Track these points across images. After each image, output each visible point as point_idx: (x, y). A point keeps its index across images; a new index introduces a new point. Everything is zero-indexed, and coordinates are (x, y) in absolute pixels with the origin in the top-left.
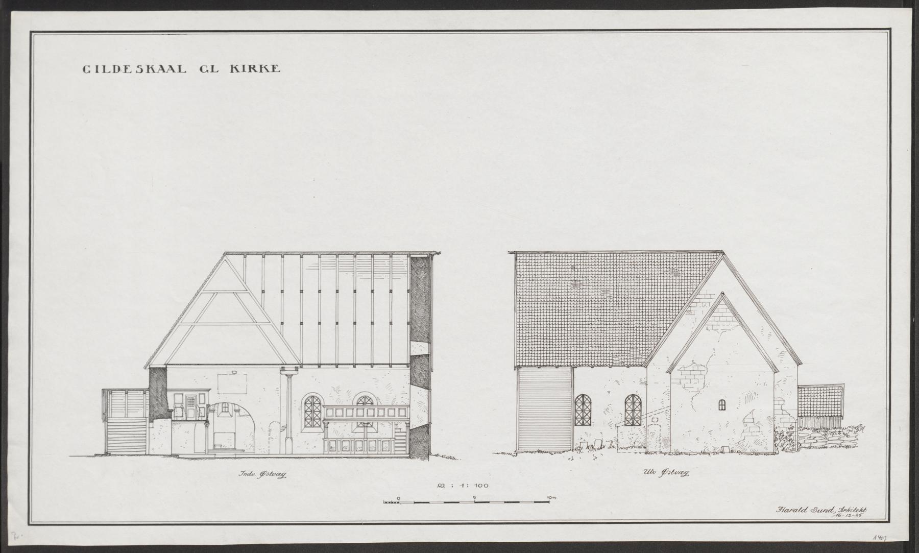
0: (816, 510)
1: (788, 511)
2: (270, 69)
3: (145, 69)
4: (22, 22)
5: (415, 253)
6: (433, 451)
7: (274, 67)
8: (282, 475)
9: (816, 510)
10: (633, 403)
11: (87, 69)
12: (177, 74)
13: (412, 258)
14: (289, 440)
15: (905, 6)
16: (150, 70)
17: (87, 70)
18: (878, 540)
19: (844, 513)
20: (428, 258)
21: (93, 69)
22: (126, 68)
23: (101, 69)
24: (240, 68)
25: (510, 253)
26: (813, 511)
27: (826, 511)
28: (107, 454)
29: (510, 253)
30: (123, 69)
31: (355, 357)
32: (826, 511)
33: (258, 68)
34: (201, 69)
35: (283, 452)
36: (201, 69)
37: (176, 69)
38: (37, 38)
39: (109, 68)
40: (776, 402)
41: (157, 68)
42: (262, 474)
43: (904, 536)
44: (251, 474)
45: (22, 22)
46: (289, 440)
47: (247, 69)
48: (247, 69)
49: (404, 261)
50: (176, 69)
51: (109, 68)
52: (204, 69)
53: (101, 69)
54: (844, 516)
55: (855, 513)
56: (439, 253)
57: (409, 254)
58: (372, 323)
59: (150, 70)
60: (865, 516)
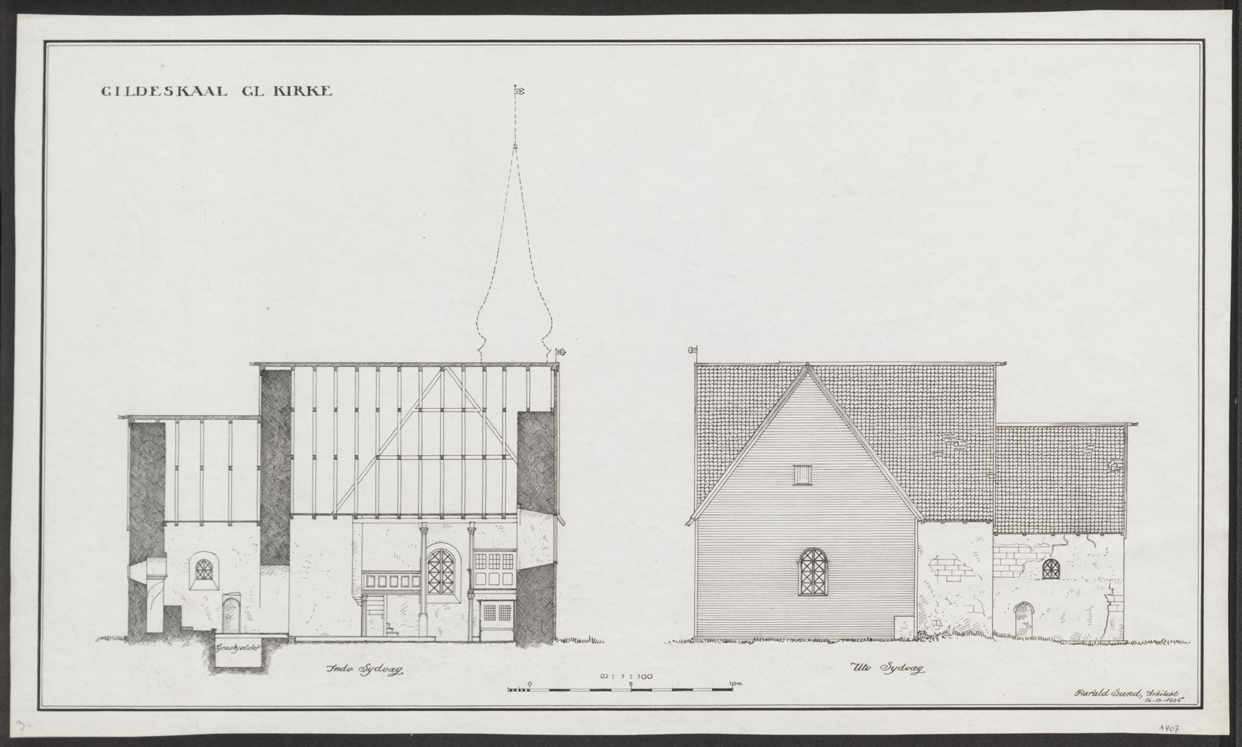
1: (1086, 694)
2: (320, 91)
3: (176, 92)
4: (32, 29)
5: (268, 364)
6: (560, 634)
7: (324, 89)
11: (107, 91)
12: (216, 97)
14: (423, 617)
19: (1154, 698)
21: (114, 91)
22: (153, 90)
24: (285, 91)
25: (251, 364)
26: (1113, 695)
27: (1095, 694)
29: (251, 364)
30: (149, 92)
31: (314, 504)
32: (1130, 694)
33: (305, 91)
34: (103, 92)
35: (423, 633)
36: (103, 92)
37: (215, 91)
38: (50, 47)
39: (133, 91)
40: (996, 550)
41: (190, 90)
42: (368, 670)
44: (347, 669)
45: (32, 29)
46: (423, 617)
47: (293, 91)
48: (293, 91)
50: (215, 91)
52: (248, 91)
53: (123, 91)
54: (1154, 701)
55: (1163, 698)
58: (315, 458)
60: (1184, 702)
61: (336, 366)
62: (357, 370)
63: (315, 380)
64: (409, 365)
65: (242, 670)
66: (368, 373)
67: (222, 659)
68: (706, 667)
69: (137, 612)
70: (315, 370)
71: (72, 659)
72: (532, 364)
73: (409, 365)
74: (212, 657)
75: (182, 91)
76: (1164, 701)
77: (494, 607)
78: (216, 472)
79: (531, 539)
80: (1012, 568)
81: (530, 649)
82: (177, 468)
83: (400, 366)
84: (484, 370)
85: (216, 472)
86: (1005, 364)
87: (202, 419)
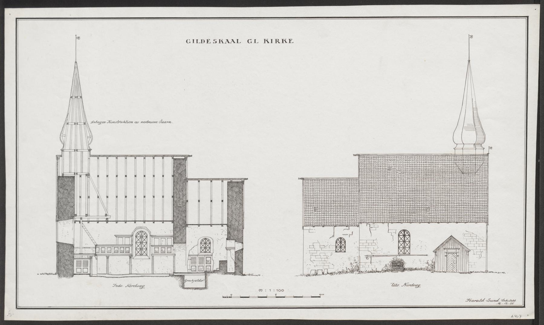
0: (489, 300)
2: (288, 41)
3: (218, 41)
5: (176, 156)
8: (142, 287)
9: (489, 300)
10: (341, 242)
12: (236, 44)
13: (174, 159)
15: (537, 3)
16: (266, 42)
17: (188, 42)
18: (514, 318)
20: (186, 158)
22: (208, 41)
23: (195, 41)
25: (355, 155)
27: (495, 301)
28: (487, 271)
29: (355, 155)
30: (206, 41)
31: (144, 216)
32: (495, 301)
37: (236, 41)
38: (19, 22)
39: (199, 41)
41: (224, 41)
43: (532, 317)
45: (11, 14)
48: (274, 41)
49: (169, 162)
50: (236, 41)
51: (199, 41)
53: (195, 41)
54: (503, 304)
55: (510, 303)
56: (191, 156)
57: (173, 156)
59: (266, 42)
60: (515, 304)
61: (135, 157)
62: (98, 159)
63: (144, 163)
64: (139, 156)
65: (196, 289)
66: (131, 160)
67: (187, 285)
68: (310, 287)
69: (239, 264)
70: (154, 158)
71: (32, 285)
72: (99, 156)
73: (139, 156)
74: (183, 284)
75: (277, 41)
76: (509, 304)
77: (81, 261)
78: (205, 202)
79: (68, 232)
80: (476, 245)
81: (64, 279)
82: (222, 201)
83: (163, 156)
84: (154, 158)
85: (205, 202)
86: (191, 156)
87: (199, 180)
